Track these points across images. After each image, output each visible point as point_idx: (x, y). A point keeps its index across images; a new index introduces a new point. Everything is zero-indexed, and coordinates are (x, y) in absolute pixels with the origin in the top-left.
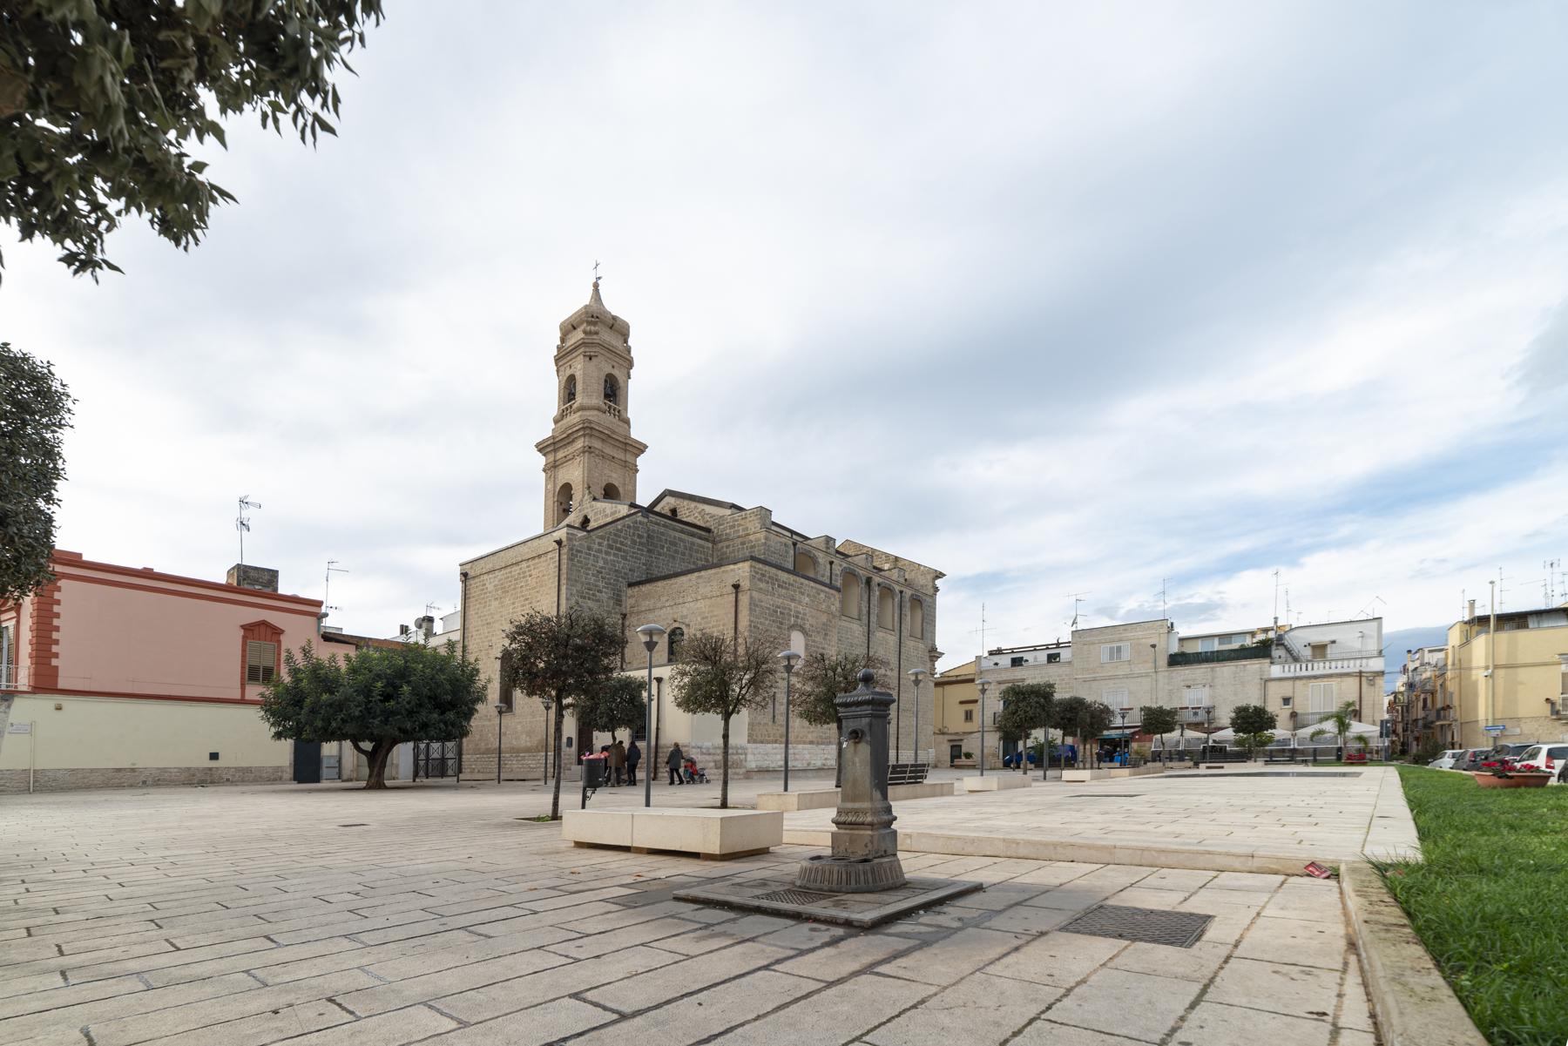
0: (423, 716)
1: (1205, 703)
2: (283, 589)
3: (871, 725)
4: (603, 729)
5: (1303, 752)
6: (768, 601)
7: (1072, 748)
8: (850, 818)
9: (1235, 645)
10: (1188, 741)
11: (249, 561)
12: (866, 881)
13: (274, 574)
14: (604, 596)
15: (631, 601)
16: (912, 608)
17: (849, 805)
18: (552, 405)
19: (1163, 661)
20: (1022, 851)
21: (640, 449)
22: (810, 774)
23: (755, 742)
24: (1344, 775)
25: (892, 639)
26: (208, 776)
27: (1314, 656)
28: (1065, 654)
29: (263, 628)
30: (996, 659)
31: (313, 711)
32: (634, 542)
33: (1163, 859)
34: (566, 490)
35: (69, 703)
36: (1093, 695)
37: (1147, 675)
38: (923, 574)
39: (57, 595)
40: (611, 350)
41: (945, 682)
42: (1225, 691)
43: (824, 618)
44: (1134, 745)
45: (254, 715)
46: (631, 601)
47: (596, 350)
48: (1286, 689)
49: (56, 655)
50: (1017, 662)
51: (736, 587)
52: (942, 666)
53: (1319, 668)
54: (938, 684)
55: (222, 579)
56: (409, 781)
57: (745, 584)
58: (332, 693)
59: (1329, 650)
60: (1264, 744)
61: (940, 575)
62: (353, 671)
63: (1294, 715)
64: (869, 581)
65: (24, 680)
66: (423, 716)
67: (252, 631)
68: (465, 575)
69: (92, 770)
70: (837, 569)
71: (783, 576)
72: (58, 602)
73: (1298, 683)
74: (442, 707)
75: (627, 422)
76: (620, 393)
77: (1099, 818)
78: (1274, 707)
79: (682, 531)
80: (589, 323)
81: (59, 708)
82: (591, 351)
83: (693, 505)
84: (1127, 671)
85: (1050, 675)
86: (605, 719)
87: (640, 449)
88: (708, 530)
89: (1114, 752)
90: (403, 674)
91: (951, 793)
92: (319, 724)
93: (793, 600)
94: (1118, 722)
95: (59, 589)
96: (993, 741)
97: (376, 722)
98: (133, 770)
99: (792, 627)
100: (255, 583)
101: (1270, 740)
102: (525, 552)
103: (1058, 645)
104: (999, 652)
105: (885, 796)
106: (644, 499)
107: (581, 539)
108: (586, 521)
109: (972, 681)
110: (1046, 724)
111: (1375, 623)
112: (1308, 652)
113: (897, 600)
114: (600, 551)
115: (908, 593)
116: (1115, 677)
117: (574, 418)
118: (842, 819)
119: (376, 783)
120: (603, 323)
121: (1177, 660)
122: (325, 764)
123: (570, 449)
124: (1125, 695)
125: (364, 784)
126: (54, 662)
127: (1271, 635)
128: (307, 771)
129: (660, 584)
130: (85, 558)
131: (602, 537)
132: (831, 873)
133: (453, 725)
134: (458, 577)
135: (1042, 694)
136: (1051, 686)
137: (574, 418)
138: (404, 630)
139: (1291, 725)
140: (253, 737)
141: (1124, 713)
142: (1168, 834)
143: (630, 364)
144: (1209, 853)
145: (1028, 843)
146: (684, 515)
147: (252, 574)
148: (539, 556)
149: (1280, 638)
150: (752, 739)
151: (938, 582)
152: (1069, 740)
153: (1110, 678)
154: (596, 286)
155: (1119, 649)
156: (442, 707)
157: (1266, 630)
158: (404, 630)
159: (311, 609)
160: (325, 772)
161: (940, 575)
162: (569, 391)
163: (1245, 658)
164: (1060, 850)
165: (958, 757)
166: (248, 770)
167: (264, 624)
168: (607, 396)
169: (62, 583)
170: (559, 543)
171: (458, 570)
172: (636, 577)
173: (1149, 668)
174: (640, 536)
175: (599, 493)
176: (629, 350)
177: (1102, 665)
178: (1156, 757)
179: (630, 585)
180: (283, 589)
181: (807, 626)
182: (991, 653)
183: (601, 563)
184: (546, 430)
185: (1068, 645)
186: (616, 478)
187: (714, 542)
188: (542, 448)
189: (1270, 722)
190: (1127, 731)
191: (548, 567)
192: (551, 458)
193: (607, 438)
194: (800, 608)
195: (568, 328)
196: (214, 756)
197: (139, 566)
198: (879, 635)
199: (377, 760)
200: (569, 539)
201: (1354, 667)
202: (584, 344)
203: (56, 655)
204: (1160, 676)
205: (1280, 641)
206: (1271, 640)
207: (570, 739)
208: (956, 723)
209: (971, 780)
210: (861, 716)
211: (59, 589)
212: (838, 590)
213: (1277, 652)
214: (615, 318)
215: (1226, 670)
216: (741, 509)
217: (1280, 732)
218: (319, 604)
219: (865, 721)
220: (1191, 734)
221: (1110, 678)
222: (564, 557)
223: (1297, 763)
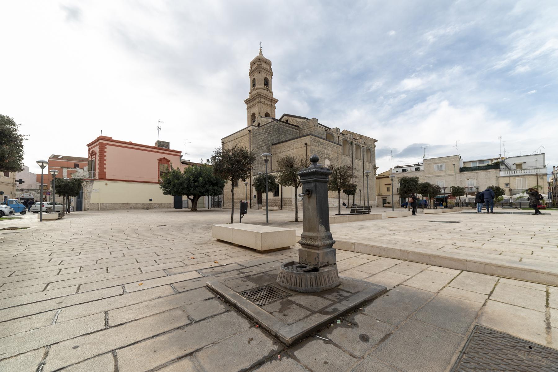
0: (207, 187)
1: (475, 185)
2: (171, 148)
3: (316, 186)
5: (514, 204)
7: (426, 201)
8: (308, 242)
9: (485, 164)
10: (469, 199)
11: (161, 140)
12: (312, 285)
13: (168, 143)
14: (264, 148)
15: (273, 150)
16: (367, 153)
17: (307, 234)
18: (249, 89)
19: (458, 170)
20: (411, 257)
21: (276, 101)
22: (334, 209)
25: (361, 163)
26: (148, 207)
27: (517, 168)
28: (421, 168)
30: (397, 169)
31: (174, 186)
32: (273, 130)
33: (499, 271)
34: (254, 115)
35: (109, 183)
36: (434, 182)
37: (452, 175)
39: (105, 150)
40: (265, 70)
41: (380, 178)
42: (484, 181)
43: (336, 155)
44: (449, 201)
45: (158, 186)
46: (273, 150)
47: (261, 69)
48: (507, 180)
49: (105, 168)
51: (306, 144)
52: (378, 172)
53: (519, 173)
54: (377, 178)
56: (207, 209)
57: (309, 143)
58: (178, 180)
59: (523, 166)
60: (500, 201)
61: (376, 141)
62: (185, 173)
63: (510, 190)
64: (352, 143)
65: (97, 177)
66: (207, 187)
67: (161, 160)
68: (223, 142)
70: (341, 139)
71: (322, 141)
73: (511, 178)
74: (213, 184)
75: (272, 93)
76: (270, 83)
77: (447, 236)
78: (502, 186)
79: (289, 127)
80: (259, 62)
81: (106, 185)
82: (259, 70)
83: (293, 118)
84: (444, 174)
85: (417, 174)
87: (276, 101)
88: (298, 127)
89: (441, 202)
90: (200, 174)
91: (381, 218)
92: (175, 190)
93: (325, 149)
94: (443, 192)
96: (397, 198)
99: (325, 158)
100: (162, 146)
101: (502, 199)
103: (419, 165)
104: (398, 167)
105: (328, 229)
106: (278, 117)
108: (259, 124)
109: (388, 177)
110: (415, 193)
111: (542, 156)
112: (515, 167)
113: (362, 149)
115: (365, 147)
116: (440, 176)
117: (255, 92)
118: (304, 242)
119: (194, 209)
120: (263, 61)
121: (462, 170)
122: (183, 203)
123: (254, 102)
124: (445, 182)
125: (190, 209)
126: (105, 170)
127: (499, 160)
128: (178, 205)
129: (282, 144)
132: (291, 278)
133: (217, 190)
134: (221, 143)
135: (414, 181)
136: (418, 178)
137: (255, 92)
138: (208, 161)
139: (509, 193)
140: (156, 193)
141: (445, 189)
142: (494, 251)
143: (272, 74)
144: (534, 271)
145: (414, 253)
146: (290, 122)
147: (162, 143)
149: (503, 161)
151: (375, 143)
152: (425, 198)
153: (438, 176)
154: (261, 50)
155: (441, 166)
156: (213, 184)
157: (497, 159)
158: (208, 161)
159: (178, 154)
160: (183, 205)
161: (376, 141)
162: (254, 84)
163: (490, 169)
164: (432, 259)
165: (385, 203)
166: (161, 204)
167: (164, 159)
168: (265, 85)
169: (107, 146)
170: (250, 131)
171: (221, 141)
172: (275, 142)
173: (452, 172)
175: (263, 115)
178: (457, 205)
179: (273, 145)
182: (395, 168)
183: (263, 137)
184: (247, 96)
185: (422, 164)
186: (269, 111)
187: (300, 130)
188: (246, 102)
189: (503, 193)
190: (446, 195)
193: (265, 98)
194: (328, 152)
195: (253, 63)
196: (151, 200)
197: (128, 141)
198: (356, 161)
199: (194, 201)
201: (534, 172)
202: (257, 68)
204: (457, 175)
205: (503, 163)
206: (499, 162)
208: (384, 192)
209: (389, 212)
210: (311, 182)
212: (341, 146)
213: (502, 167)
214: (266, 60)
215: (482, 173)
217: (506, 197)
218: (180, 152)
219: (313, 185)
220: (470, 196)
221: (438, 176)
223: (513, 208)
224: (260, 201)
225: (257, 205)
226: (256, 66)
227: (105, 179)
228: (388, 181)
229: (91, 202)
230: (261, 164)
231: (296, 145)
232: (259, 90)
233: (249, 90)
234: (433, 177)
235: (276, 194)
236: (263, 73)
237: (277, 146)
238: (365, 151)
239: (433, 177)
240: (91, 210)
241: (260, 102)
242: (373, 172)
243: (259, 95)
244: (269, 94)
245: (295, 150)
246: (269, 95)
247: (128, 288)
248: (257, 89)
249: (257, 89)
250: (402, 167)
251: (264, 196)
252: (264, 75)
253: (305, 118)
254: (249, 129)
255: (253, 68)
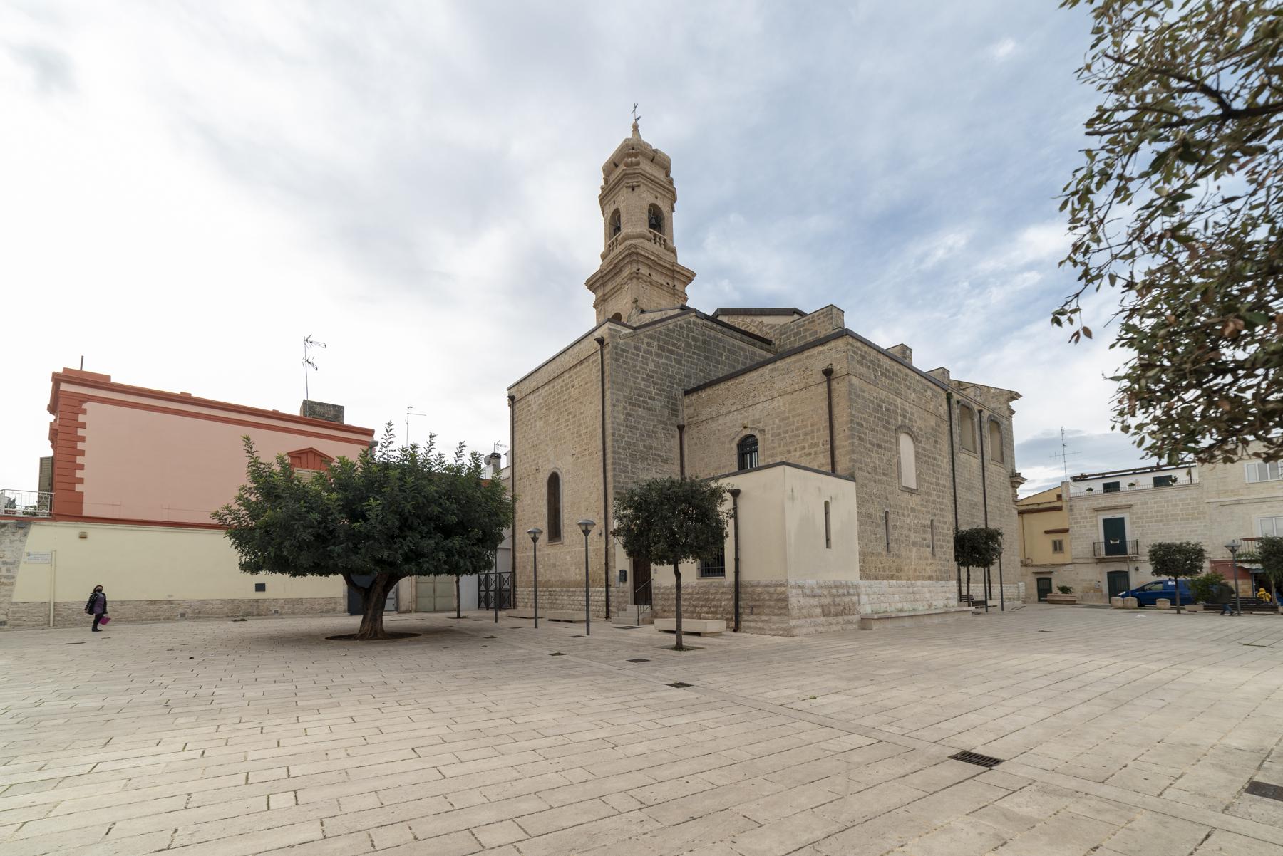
4: (661, 560)
6: (871, 392)
11: (313, 398)
16: (991, 431)
23: (868, 578)
24: (737, 560)
25: (975, 462)
29: (311, 456)
32: (688, 345)
35: (94, 531)
38: (994, 396)
41: (1028, 510)
46: (691, 411)
47: (638, 183)
50: (1111, 488)
52: (1023, 492)
55: (296, 411)
61: (1014, 396)
68: (511, 398)
69: (123, 603)
72: (83, 426)
75: (674, 251)
80: (630, 155)
81: (83, 537)
82: (633, 182)
86: (663, 545)
88: (769, 342)
93: (898, 394)
95: (84, 412)
97: (338, 549)
98: (170, 602)
99: (899, 429)
102: (567, 360)
104: (1082, 478)
107: (626, 336)
114: (649, 352)
120: (644, 154)
123: (618, 280)
126: (78, 488)
129: (722, 386)
130: (113, 380)
131: (650, 337)
134: (506, 401)
147: (318, 409)
148: (581, 362)
150: (865, 575)
151: (1013, 404)
154: (636, 127)
161: (1014, 396)
162: (614, 225)
166: (299, 601)
167: (311, 451)
168: (651, 226)
170: (601, 341)
172: (693, 383)
174: (695, 339)
176: (671, 182)
177: (1248, 486)
179: (687, 393)
180: (349, 420)
181: (915, 429)
183: (651, 366)
188: (592, 284)
191: (590, 372)
192: (600, 293)
193: (654, 264)
197: (177, 391)
200: (613, 336)
202: (625, 176)
203: (81, 481)
207: (623, 573)
208: (1043, 553)
211: (84, 412)
214: (656, 151)
216: (802, 314)
218: (370, 433)
221: (1263, 500)
222: (607, 357)
224: (643, 593)
225: (632, 609)
226: (618, 172)
227: (75, 515)
228: (1054, 521)
229: (18, 597)
230: (643, 459)
231: (782, 384)
232: (628, 243)
233: (602, 248)
234: (1238, 503)
235: (713, 567)
236: (643, 188)
237: (703, 394)
238: (986, 426)
239: (1238, 503)
240: (14, 626)
241: (636, 276)
242: (1006, 494)
243: (633, 255)
244: (668, 256)
245: (779, 402)
246: (667, 258)
247: (343, 754)
248: (625, 239)
249: (625, 239)
250: (1103, 476)
251: (662, 576)
252: (646, 197)
253: (795, 311)
254: (597, 334)
255: (613, 178)
